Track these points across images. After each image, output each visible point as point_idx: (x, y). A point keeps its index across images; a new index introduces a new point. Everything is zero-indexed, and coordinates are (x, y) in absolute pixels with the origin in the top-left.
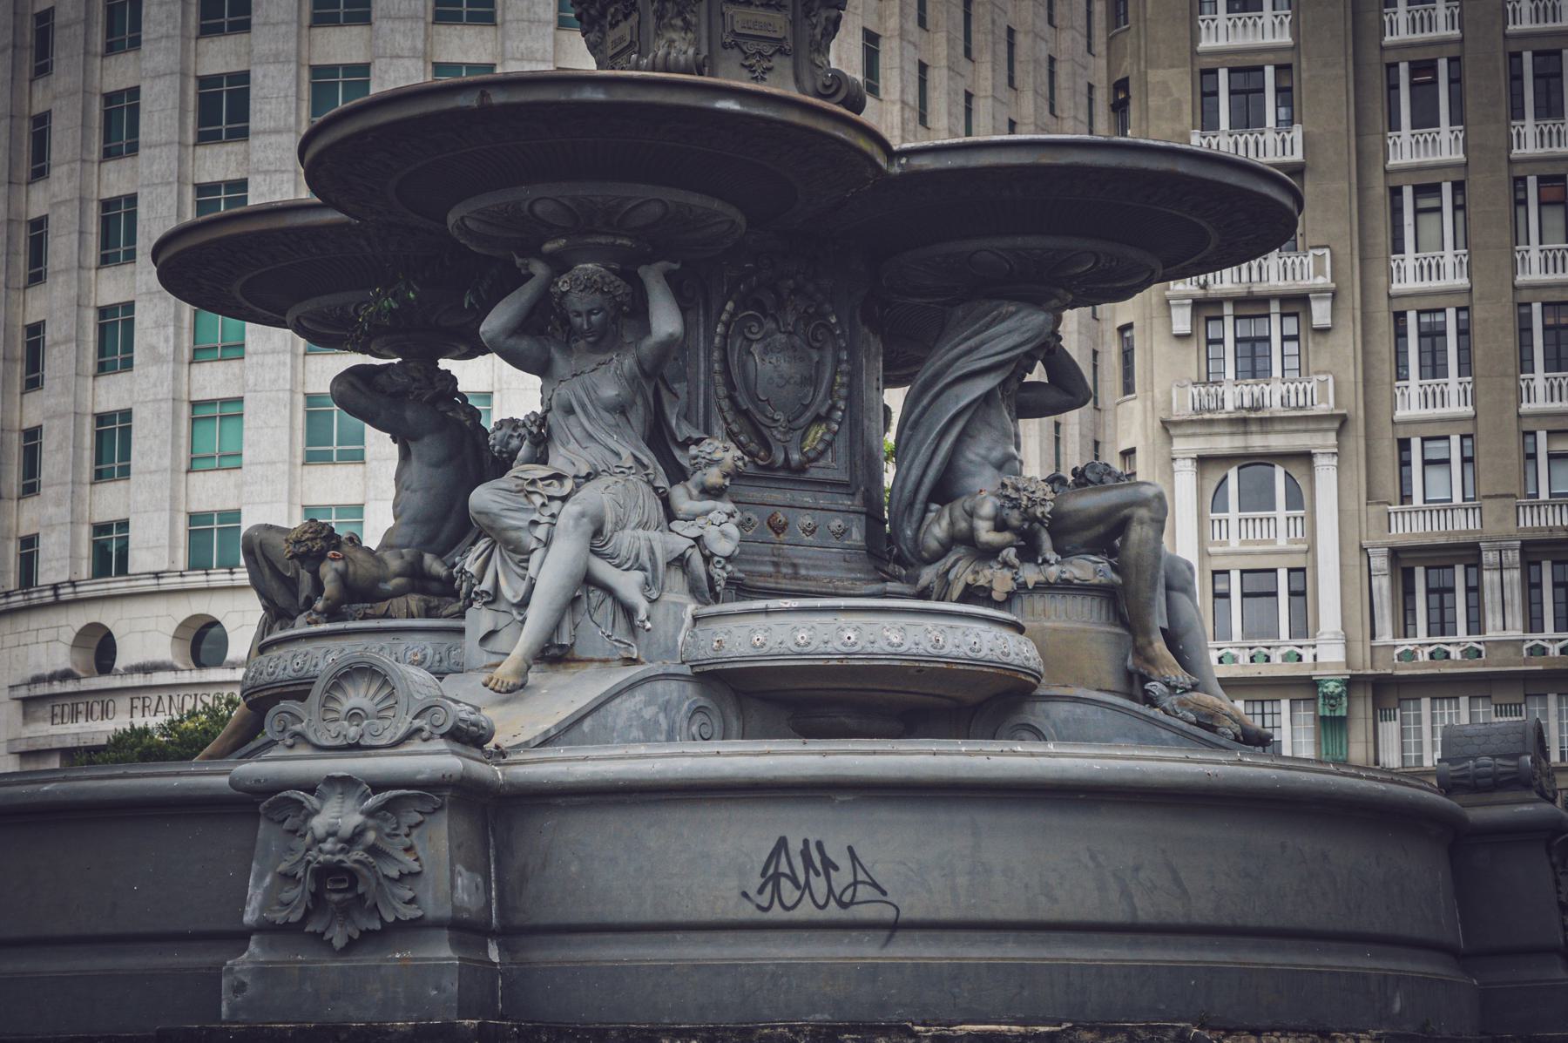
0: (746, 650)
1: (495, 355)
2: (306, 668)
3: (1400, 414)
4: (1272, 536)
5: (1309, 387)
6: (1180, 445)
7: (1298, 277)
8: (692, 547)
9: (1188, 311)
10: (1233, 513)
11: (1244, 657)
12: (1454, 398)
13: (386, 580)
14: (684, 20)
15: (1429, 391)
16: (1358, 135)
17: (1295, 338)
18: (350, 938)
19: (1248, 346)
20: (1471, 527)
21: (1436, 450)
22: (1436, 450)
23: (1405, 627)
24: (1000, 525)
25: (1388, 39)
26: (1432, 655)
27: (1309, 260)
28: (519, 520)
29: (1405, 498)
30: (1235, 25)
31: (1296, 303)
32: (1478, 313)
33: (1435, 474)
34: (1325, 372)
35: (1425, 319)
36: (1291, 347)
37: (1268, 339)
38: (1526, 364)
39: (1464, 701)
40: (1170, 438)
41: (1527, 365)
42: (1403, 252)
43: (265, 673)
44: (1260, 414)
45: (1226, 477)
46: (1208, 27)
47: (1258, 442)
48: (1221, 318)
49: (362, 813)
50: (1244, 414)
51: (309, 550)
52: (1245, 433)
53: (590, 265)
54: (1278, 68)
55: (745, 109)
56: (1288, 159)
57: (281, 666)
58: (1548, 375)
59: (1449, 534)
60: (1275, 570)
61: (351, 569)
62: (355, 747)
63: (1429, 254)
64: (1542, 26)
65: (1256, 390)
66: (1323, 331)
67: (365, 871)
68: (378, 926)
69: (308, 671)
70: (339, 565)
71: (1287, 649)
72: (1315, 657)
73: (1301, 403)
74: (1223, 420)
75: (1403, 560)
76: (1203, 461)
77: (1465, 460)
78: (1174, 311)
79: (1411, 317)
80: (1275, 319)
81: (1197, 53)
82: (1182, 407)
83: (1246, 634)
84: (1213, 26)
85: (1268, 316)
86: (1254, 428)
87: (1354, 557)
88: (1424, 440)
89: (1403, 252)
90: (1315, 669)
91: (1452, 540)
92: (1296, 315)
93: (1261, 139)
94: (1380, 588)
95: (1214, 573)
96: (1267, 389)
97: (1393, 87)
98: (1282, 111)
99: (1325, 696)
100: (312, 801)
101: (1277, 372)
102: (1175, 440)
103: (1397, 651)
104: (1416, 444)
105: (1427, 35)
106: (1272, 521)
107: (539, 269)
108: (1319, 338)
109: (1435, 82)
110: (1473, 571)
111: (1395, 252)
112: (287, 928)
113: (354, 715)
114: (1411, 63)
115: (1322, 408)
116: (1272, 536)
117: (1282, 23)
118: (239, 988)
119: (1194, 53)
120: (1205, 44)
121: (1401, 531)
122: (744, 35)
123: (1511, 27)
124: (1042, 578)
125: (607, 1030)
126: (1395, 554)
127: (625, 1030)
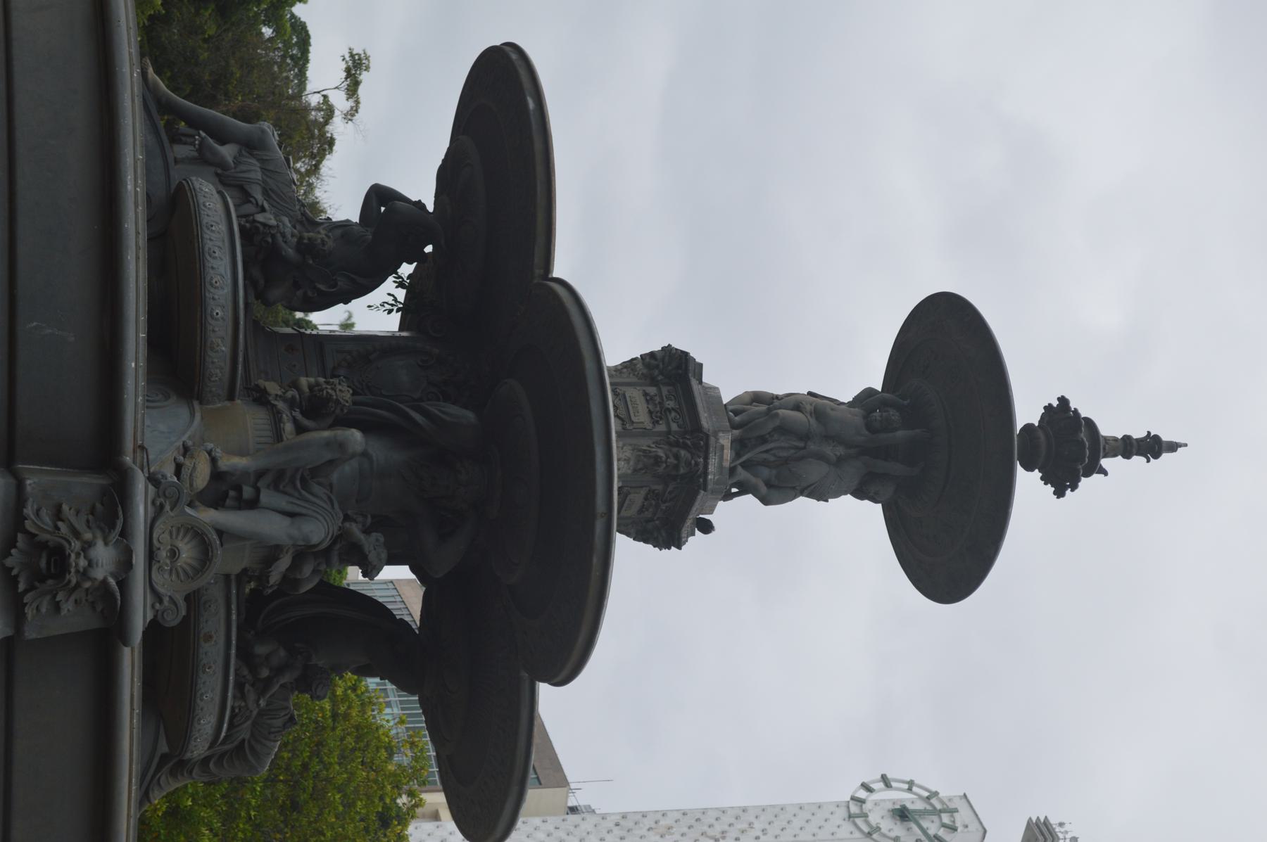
2: (212, 290)
8: (257, 204)
14: (641, 469)
18: (12, 569)
39: (126, 104)
43: (205, 199)
55: (532, 113)
57: (210, 213)
62: (151, 555)
68: (21, 587)
69: (209, 292)
100: (114, 536)
113: (174, 554)
122: (626, 402)
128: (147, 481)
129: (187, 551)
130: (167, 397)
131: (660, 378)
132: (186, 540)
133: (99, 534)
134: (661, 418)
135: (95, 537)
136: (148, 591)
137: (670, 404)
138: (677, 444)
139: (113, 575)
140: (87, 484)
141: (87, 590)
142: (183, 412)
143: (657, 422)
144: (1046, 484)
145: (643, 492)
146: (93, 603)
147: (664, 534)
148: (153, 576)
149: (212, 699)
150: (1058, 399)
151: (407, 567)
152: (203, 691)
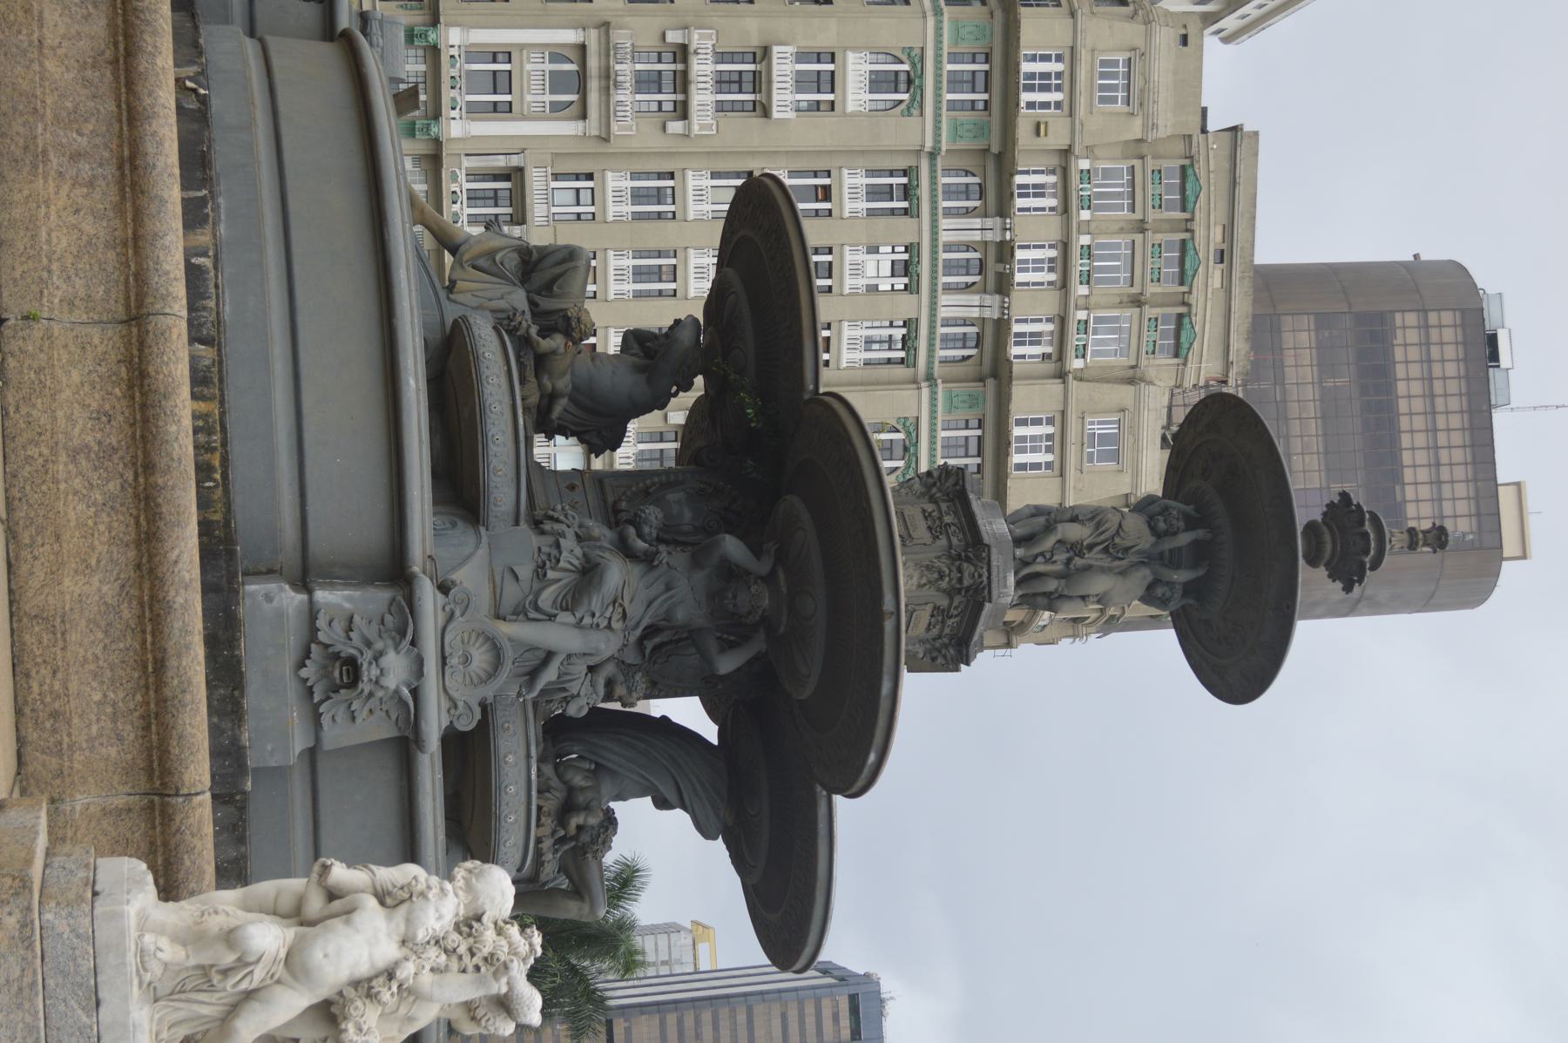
0: (502, 751)
1: (717, 727)
2: (492, 416)
3: (609, 175)
4: (532, 60)
5: (628, 119)
6: (593, 34)
7: (699, 113)
9: (681, 41)
10: (549, 67)
11: (454, 72)
12: (618, 209)
13: (550, 378)
14: (925, 584)
15: (623, 193)
16: (787, 152)
17: (660, 110)
18: (307, 679)
19: (656, 78)
20: (537, 219)
21: (585, 197)
22: (585, 197)
23: (473, 176)
24: (580, 828)
25: (846, 172)
26: (454, 192)
27: (709, 121)
28: (596, 603)
29: (556, 177)
30: (861, 75)
31: (682, 111)
32: (671, 225)
33: (571, 196)
34: (637, 129)
35: (669, 191)
36: (654, 107)
37: (660, 92)
38: (639, 254)
40: (597, 27)
41: (637, 255)
42: (712, 178)
44: (612, 87)
45: (572, 62)
46: (861, 58)
47: (594, 85)
48: (675, 62)
49: (397, 686)
50: (613, 76)
51: (573, 329)
52: (600, 77)
53: (767, 602)
54: (833, 103)
56: (775, 109)
58: (629, 189)
59: (532, 206)
60: (510, 93)
61: (559, 357)
63: (710, 195)
64: (847, 267)
65: (628, 85)
66: (664, 128)
67: (355, 693)
68: (316, 699)
70: (562, 350)
71: (459, 100)
72: (454, 119)
73: (619, 114)
74: (609, 62)
75: (515, 175)
76: (582, 48)
77: (579, 215)
78: (681, 32)
79: (671, 183)
80: (672, 97)
81: (845, 51)
82: (621, 37)
83: (470, 73)
84: (862, 61)
85: (675, 92)
86: (603, 83)
87: (517, 146)
88: (592, 189)
89: (712, 178)
90: (446, 119)
91: (528, 207)
92: (675, 111)
93: (788, 91)
94: (498, 160)
95: (510, 53)
96: (628, 92)
97: (815, 174)
98: (805, 104)
99: (429, 125)
101: (639, 97)
102: (596, 31)
103: (457, 170)
104: (590, 184)
105: (846, 196)
106: (541, 60)
107: (763, 567)
108: (660, 125)
109: (817, 200)
110: (508, 218)
111: (712, 173)
112: (314, 630)
113: (467, 660)
114: (830, 186)
115: (615, 127)
116: (532, 60)
117: (861, 105)
118: (269, 598)
119: (845, 49)
120: (851, 56)
121: (535, 174)
123: (846, 324)
124: (544, 851)
125: (245, 844)
126: (520, 170)
127: (246, 857)
128: (437, 591)
129: (480, 658)
130: (454, 525)
131: (938, 495)
132: (481, 650)
133: (390, 642)
134: (941, 534)
135: (386, 646)
136: (441, 691)
137: (948, 519)
138: (959, 557)
139: (408, 686)
140: (379, 597)
141: (381, 699)
142: (471, 539)
143: (938, 537)
144: (1334, 581)
145: (929, 608)
146: (387, 711)
147: (952, 651)
148: (447, 683)
149: (516, 821)
150: (1340, 494)
151: (696, 700)
152: (506, 838)
